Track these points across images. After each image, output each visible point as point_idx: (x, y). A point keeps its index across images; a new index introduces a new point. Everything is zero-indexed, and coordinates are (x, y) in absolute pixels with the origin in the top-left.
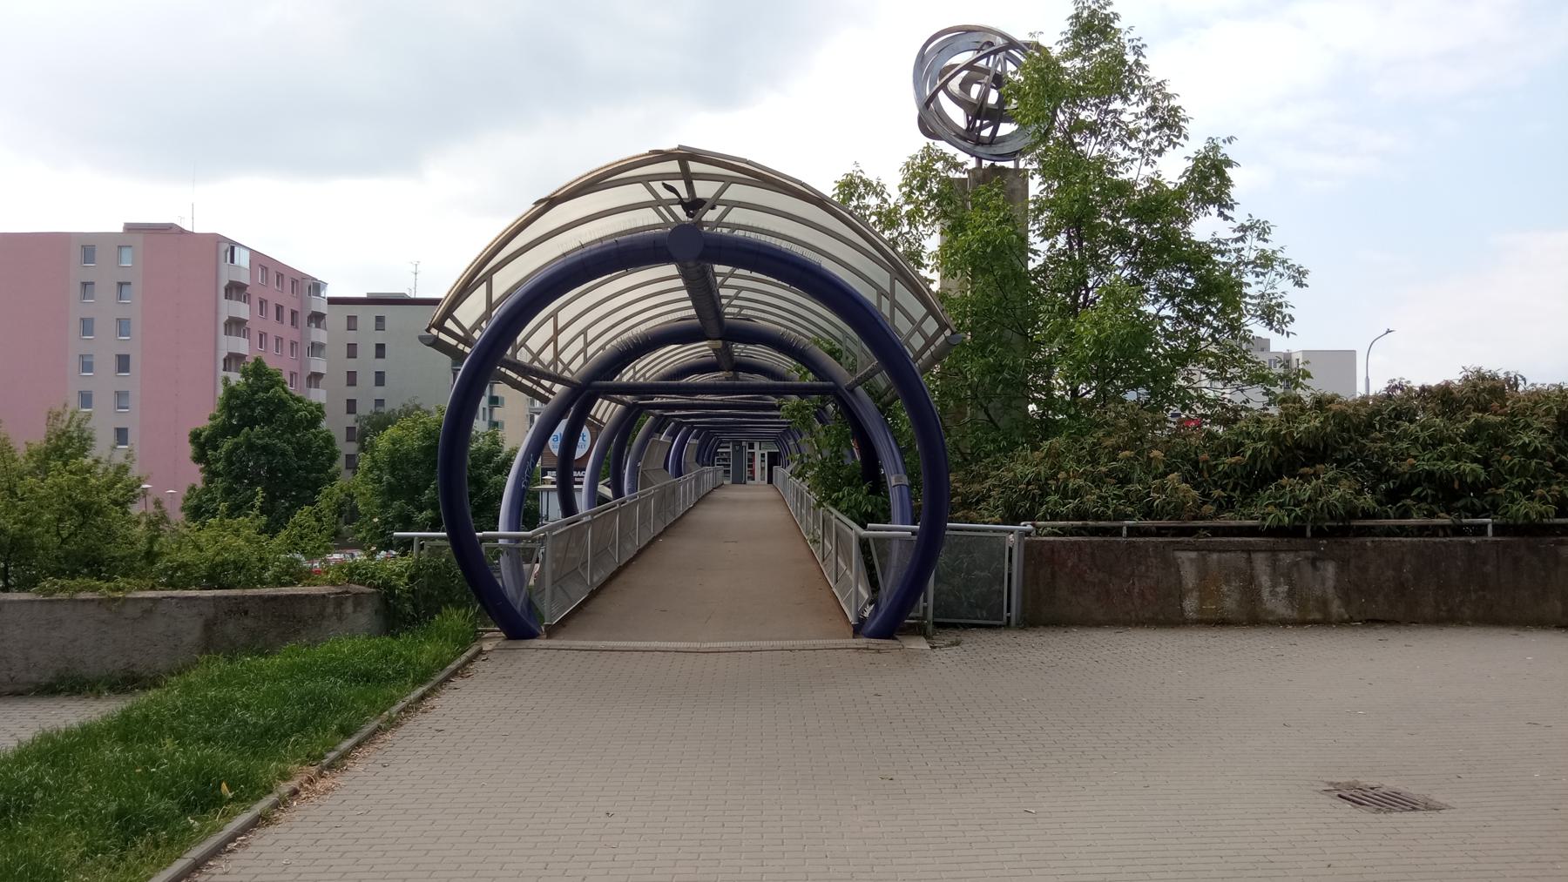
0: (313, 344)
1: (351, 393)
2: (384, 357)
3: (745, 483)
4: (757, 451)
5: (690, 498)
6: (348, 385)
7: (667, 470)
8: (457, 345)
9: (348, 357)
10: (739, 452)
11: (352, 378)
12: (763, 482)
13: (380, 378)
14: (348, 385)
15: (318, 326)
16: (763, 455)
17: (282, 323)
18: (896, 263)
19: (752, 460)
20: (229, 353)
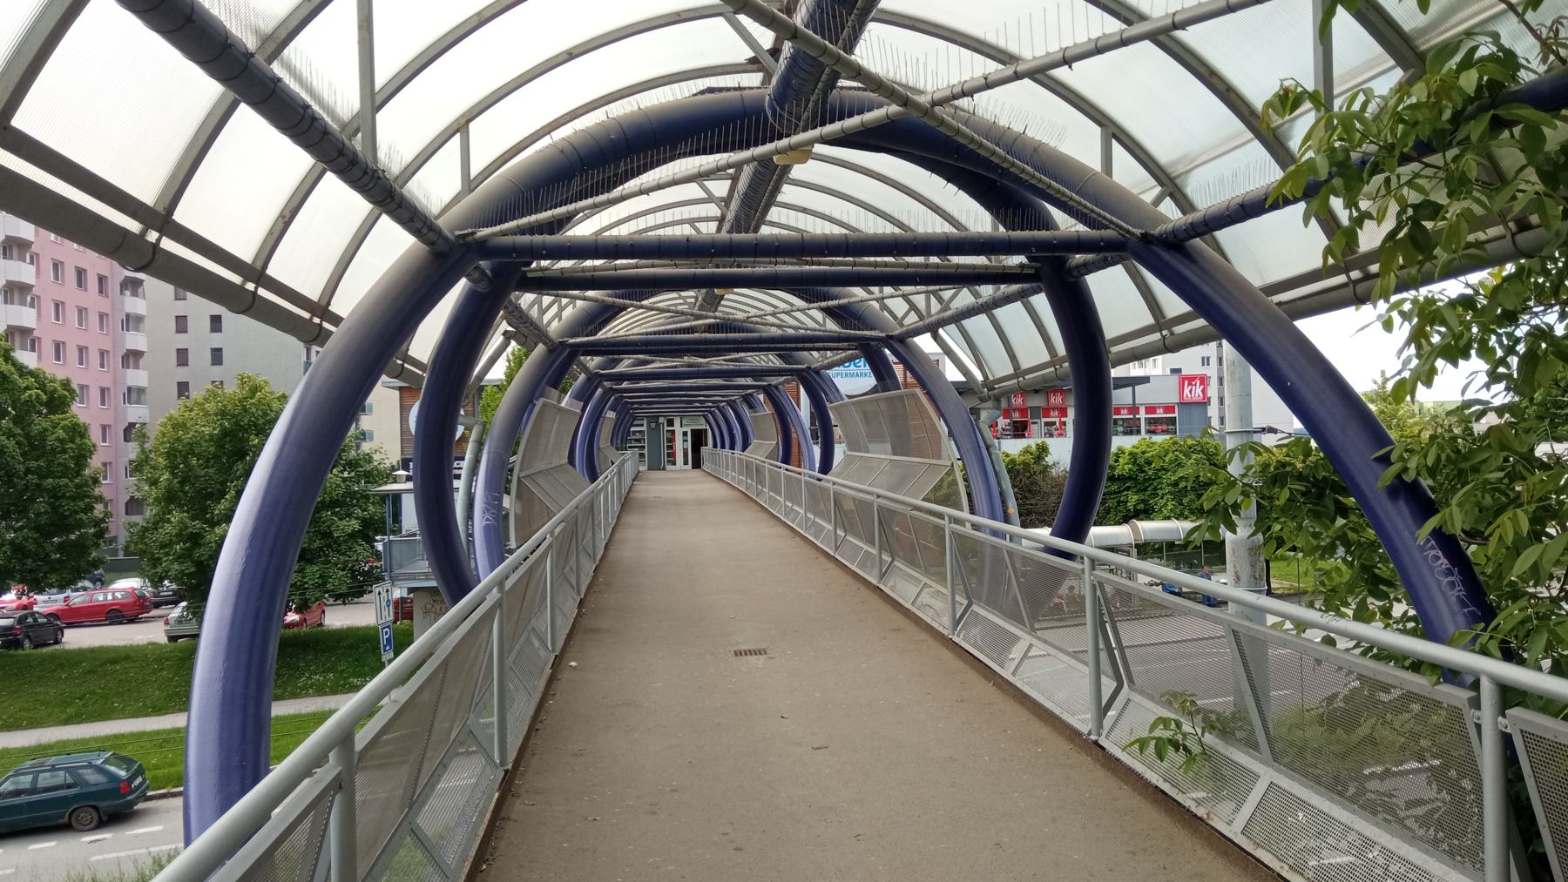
0: (128, 316)
1: (182, 374)
2: (220, 331)
3: (664, 469)
4: (678, 429)
5: (612, 507)
6: (178, 365)
7: (573, 465)
8: (256, 288)
9: (178, 332)
10: (655, 430)
11: (182, 357)
12: (686, 467)
13: (217, 356)
14: (178, 365)
15: (135, 294)
16: (685, 434)
17: (86, 290)
18: (671, 342)
19: (671, 440)
20: (9, 327)
